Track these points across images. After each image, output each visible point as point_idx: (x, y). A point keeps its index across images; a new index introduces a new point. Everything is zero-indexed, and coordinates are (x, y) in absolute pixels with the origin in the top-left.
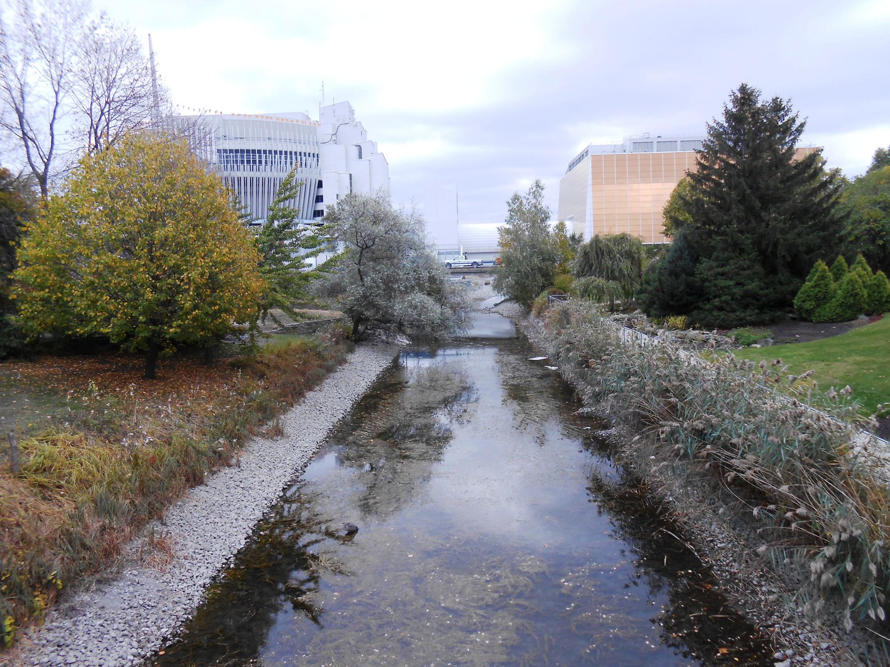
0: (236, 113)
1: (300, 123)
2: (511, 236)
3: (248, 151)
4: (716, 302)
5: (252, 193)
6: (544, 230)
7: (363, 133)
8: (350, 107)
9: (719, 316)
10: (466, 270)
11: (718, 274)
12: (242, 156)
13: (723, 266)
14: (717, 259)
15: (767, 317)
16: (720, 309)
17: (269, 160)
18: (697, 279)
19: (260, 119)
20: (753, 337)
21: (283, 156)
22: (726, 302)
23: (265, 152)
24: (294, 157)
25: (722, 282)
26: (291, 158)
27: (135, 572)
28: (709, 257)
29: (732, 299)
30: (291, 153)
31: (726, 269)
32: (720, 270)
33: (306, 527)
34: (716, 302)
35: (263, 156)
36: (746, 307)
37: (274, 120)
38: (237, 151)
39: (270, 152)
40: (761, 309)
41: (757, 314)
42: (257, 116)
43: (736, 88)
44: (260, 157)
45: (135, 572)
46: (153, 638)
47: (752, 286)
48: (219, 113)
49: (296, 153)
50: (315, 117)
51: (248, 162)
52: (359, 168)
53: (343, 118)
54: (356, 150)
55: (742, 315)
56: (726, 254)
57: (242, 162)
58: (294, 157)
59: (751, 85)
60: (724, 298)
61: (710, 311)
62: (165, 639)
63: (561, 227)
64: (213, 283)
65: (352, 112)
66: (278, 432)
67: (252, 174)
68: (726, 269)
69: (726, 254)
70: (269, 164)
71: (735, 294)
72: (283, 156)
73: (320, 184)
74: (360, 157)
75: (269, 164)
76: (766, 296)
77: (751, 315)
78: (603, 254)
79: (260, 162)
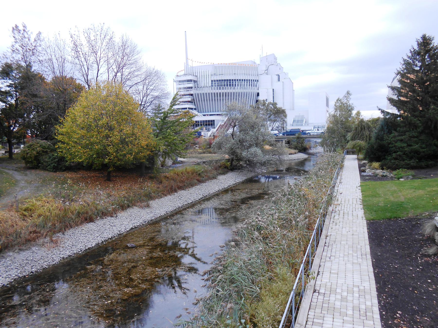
0: (220, 63)
1: (250, 66)
2: (335, 120)
3: (230, 80)
4: (394, 155)
5: (220, 100)
6: (350, 116)
7: (281, 68)
8: (275, 56)
9: (395, 163)
10: (315, 136)
11: (398, 140)
12: (230, 83)
13: (402, 135)
14: (399, 132)
15: (423, 164)
16: (396, 159)
17: (239, 84)
18: (385, 142)
19: (231, 65)
20: (403, 174)
21: (246, 82)
22: (400, 156)
23: (237, 80)
24: (251, 82)
25: (399, 144)
26: (247, 83)
27: (37, 249)
28: (395, 130)
29: (404, 154)
30: (249, 80)
31: (403, 137)
32: (400, 138)
33: (185, 251)
34: (394, 155)
35: (237, 82)
36: (411, 158)
37: (237, 65)
38: (225, 80)
39: (240, 80)
40: (420, 159)
41: (417, 162)
42: (229, 64)
43: (419, 37)
44: (235, 82)
45: (37, 249)
46: (27, 271)
47: (416, 147)
48: (212, 64)
49: (249, 80)
50: (258, 62)
51: (230, 85)
52: (278, 86)
53: (271, 62)
54: (277, 77)
55: (408, 162)
56: (405, 129)
57: (227, 85)
58: (251, 82)
59: (428, 34)
60: (398, 153)
61: (390, 160)
62: (32, 272)
63: (358, 114)
64: (123, 142)
65: (276, 59)
66: (148, 206)
67: (234, 91)
68: (403, 137)
69: (405, 129)
70: (239, 86)
71: (406, 151)
72: (246, 82)
73: (258, 94)
74: (279, 80)
75: (239, 86)
76: (424, 152)
77: (413, 163)
78: (364, 128)
79: (235, 85)
